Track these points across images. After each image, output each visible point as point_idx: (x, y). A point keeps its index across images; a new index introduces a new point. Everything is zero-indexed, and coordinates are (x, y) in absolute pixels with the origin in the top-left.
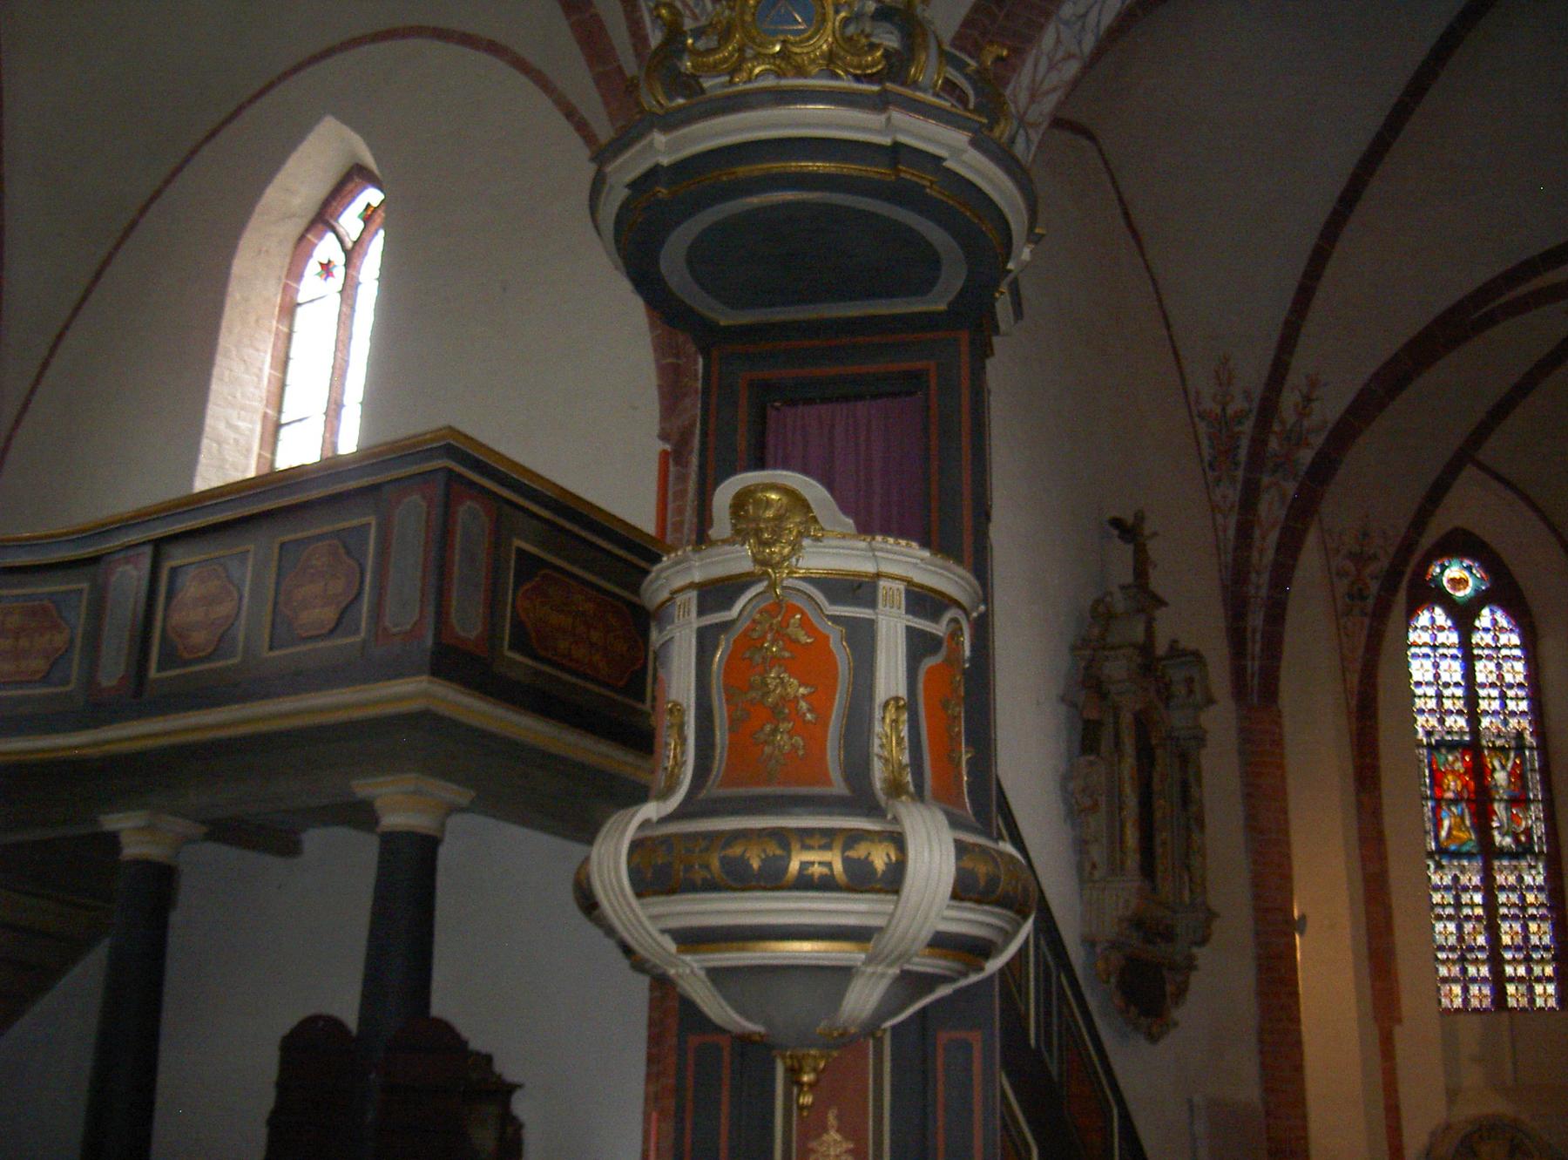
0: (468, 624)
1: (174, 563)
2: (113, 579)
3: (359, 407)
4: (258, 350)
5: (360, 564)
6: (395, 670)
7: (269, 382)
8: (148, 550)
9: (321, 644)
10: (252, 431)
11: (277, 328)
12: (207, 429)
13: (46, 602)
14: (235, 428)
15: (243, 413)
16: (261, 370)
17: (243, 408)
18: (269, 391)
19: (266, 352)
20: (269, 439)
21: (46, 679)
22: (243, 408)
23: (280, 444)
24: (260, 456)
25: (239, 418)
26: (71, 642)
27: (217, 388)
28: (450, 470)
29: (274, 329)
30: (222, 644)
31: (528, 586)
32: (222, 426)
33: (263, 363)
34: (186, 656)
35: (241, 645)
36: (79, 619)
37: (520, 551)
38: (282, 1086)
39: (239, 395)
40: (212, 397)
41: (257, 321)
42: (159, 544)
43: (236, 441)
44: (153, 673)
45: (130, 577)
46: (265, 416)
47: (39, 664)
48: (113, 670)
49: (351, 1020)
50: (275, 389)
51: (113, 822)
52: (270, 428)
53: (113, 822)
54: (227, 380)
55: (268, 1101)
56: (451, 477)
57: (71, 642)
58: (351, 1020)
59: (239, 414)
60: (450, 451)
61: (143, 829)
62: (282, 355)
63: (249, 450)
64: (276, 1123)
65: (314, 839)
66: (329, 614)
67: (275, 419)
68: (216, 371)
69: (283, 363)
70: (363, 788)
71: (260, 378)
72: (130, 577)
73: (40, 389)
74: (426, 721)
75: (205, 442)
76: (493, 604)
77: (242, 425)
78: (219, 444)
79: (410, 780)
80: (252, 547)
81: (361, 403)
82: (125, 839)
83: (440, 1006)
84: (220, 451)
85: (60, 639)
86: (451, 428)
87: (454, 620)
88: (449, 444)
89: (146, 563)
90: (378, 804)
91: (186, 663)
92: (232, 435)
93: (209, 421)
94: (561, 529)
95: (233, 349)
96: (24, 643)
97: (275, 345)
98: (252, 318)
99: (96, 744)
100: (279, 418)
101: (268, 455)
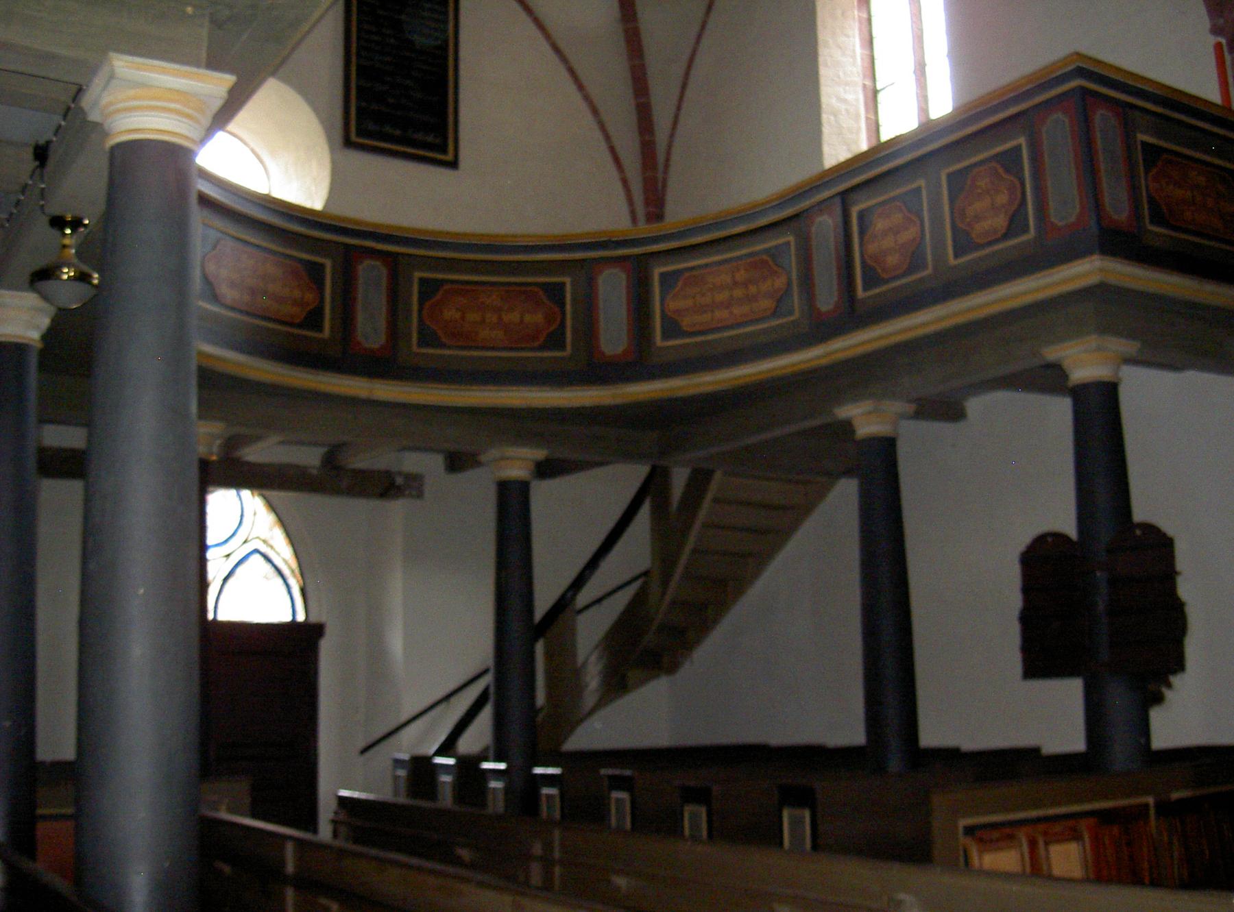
0: (1118, 205)
1: (862, 206)
2: (813, 229)
3: (947, 59)
4: (848, 36)
5: (1020, 179)
6: (1069, 253)
7: (862, 59)
8: (838, 200)
9: (1001, 246)
10: (857, 100)
11: (859, 16)
12: (824, 106)
13: (765, 257)
14: (845, 101)
15: (847, 88)
16: (854, 51)
17: (847, 84)
18: (863, 66)
19: (854, 37)
20: (871, 105)
21: (775, 313)
22: (847, 84)
23: (879, 106)
24: (867, 119)
25: (845, 92)
26: (789, 284)
27: (825, 73)
28: (1082, 88)
29: (856, 17)
30: (915, 262)
31: (1155, 171)
32: (834, 101)
33: (854, 46)
34: (885, 276)
35: (929, 258)
36: (792, 261)
37: (1143, 143)
38: (1026, 590)
39: (841, 74)
40: (823, 81)
41: (843, 14)
42: (844, 195)
43: (847, 111)
44: (860, 293)
45: (826, 225)
46: (864, 86)
47: (766, 304)
48: (827, 298)
49: (1071, 530)
50: (867, 60)
51: (847, 411)
52: (870, 94)
53: (847, 411)
54: (829, 64)
55: (1015, 600)
56: (1084, 91)
57: (789, 284)
58: (1071, 530)
59: (844, 89)
60: (1081, 72)
61: (870, 413)
62: (867, 37)
63: (857, 116)
64: (1026, 619)
65: (975, 406)
66: (1000, 222)
67: (872, 88)
68: (821, 59)
69: (869, 42)
70: (1052, 353)
71: (854, 57)
72: (826, 225)
73: (685, 105)
74: (1100, 293)
75: (824, 117)
76: (1134, 189)
77: (850, 97)
78: (835, 116)
79: (1093, 340)
80: (922, 182)
81: (947, 56)
82: (856, 423)
83: (1141, 512)
84: (836, 121)
85: (780, 282)
86: (1078, 54)
87: (1108, 208)
88: (1079, 67)
89: (838, 210)
90: (1066, 364)
91: (887, 281)
92: (843, 107)
93: (824, 100)
94: (1168, 119)
95: (830, 40)
96: (753, 289)
97: (860, 30)
98: (839, 12)
99: (829, 354)
100: (875, 87)
101: (873, 117)
